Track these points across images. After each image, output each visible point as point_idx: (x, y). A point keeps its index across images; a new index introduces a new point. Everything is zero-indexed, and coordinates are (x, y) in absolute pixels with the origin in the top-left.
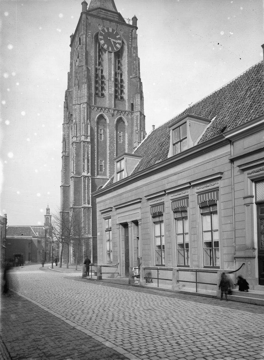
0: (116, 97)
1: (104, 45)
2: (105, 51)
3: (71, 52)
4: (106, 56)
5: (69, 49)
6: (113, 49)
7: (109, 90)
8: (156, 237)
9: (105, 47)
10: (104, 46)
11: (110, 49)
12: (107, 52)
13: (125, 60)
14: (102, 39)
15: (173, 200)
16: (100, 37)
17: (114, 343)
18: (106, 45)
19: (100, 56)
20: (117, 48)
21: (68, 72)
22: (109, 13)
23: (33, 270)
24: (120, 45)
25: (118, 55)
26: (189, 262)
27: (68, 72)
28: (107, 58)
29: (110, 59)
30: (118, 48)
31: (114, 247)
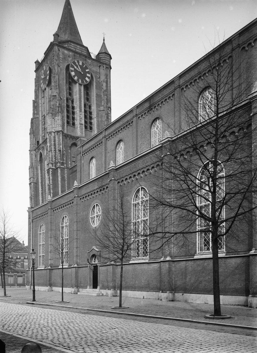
0: (86, 127)
1: (74, 76)
2: (75, 82)
3: (35, 79)
4: (76, 88)
5: (34, 75)
6: (82, 82)
7: (79, 117)
8: (121, 307)
9: (76, 78)
10: (74, 78)
11: (80, 81)
12: (78, 84)
13: (94, 93)
14: (72, 70)
15: (134, 200)
16: (71, 68)
17: (234, 42)
18: (76, 77)
19: (70, 89)
20: (86, 81)
21: (33, 100)
22: (78, 46)
23: (196, 251)
24: (89, 79)
25: (87, 88)
26: (95, 317)
27: (33, 100)
28: (77, 90)
29: (80, 90)
30: (87, 82)
31: (36, 258)
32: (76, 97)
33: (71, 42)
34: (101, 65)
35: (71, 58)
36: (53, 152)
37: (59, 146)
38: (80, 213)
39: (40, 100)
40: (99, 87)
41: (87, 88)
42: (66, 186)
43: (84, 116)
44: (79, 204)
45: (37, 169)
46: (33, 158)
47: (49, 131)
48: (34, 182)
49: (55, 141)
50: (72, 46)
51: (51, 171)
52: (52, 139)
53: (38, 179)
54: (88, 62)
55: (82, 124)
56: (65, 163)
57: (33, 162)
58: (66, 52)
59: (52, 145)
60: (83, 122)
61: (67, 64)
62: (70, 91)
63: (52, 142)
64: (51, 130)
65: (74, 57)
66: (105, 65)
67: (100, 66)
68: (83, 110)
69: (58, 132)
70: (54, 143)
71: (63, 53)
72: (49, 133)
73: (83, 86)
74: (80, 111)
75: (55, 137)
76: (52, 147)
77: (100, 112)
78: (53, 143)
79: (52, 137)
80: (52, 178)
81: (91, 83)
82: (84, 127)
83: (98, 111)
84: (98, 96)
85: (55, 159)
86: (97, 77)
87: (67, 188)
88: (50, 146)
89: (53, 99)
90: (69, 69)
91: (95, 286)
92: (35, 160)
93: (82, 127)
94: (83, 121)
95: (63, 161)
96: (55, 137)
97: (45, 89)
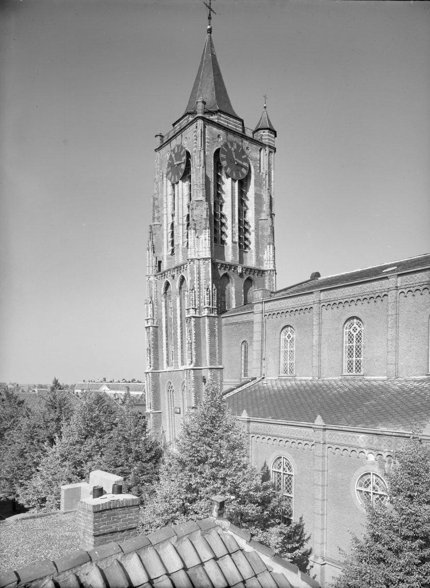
6: (237, 175)
18: (229, 169)
20: (242, 174)
25: (243, 184)
32: (227, 198)
33: (219, 111)
35: (222, 139)
36: (196, 290)
37: (206, 282)
38: (327, 471)
42: (217, 344)
45: (160, 307)
47: (190, 258)
48: (154, 325)
49: (199, 273)
50: (222, 118)
51: (194, 322)
52: (195, 269)
53: (160, 320)
54: (245, 144)
56: (215, 308)
59: (195, 279)
60: (237, 239)
61: (217, 148)
63: (195, 276)
67: (260, 151)
68: (237, 221)
70: (198, 276)
71: (211, 132)
73: (237, 182)
75: (199, 268)
76: (195, 282)
77: (260, 222)
78: (196, 276)
79: (195, 266)
80: (194, 332)
81: (248, 177)
83: (257, 221)
84: (258, 197)
85: (199, 301)
89: (197, 206)
90: (219, 156)
92: (155, 290)
93: (236, 247)
95: (212, 306)
96: (199, 268)
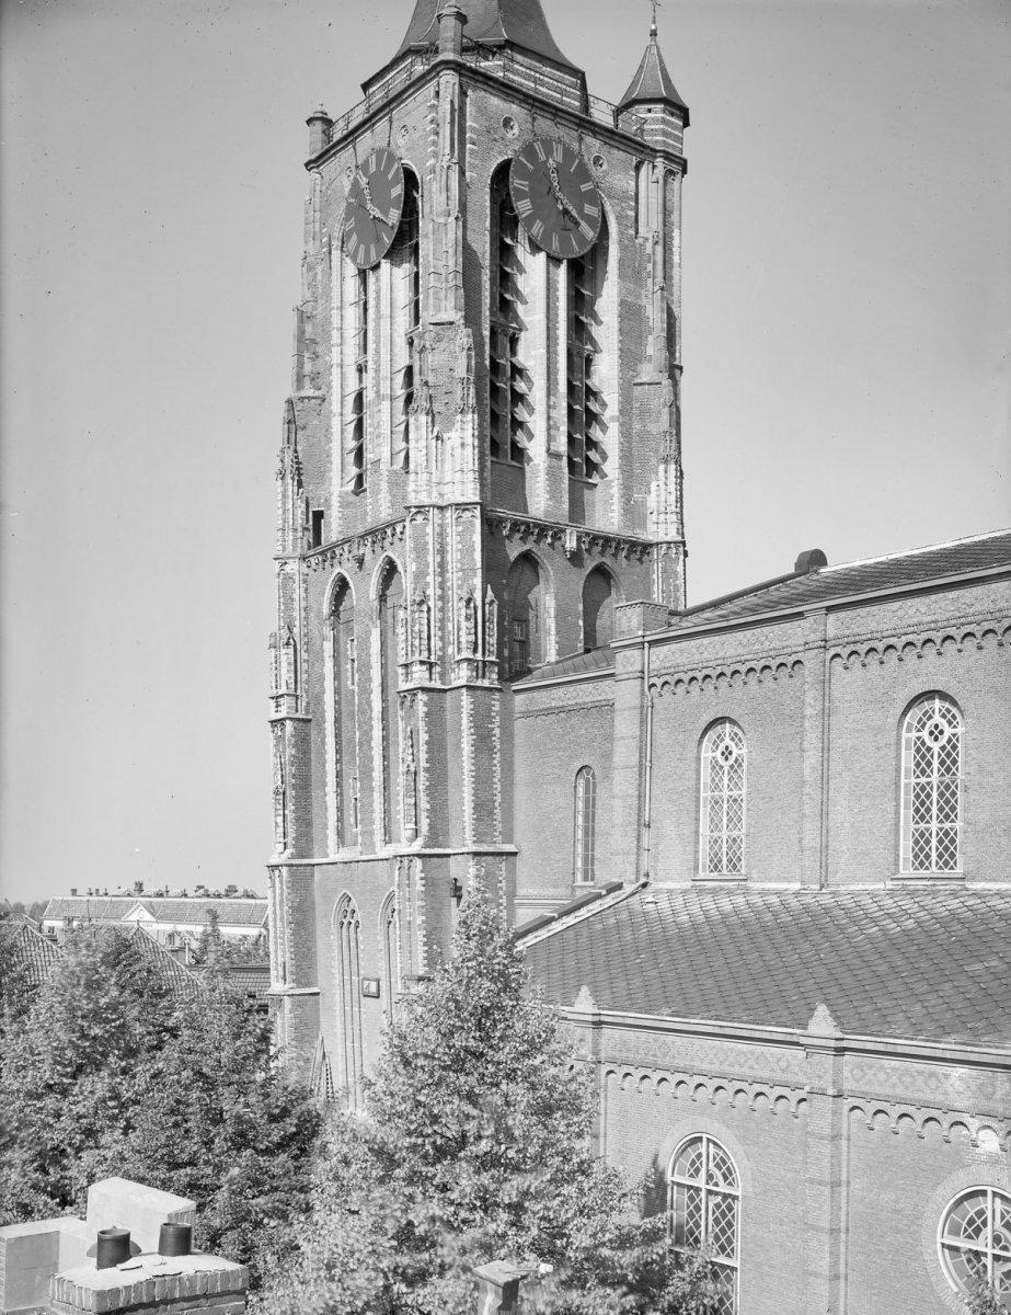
6: (564, 242)
11: (555, 244)
20: (582, 239)
25: (583, 271)
32: (531, 315)
34: (642, 156)
37: (465, 579)
39: (334, 312)
40: (632, 272)
41: (583, 271)
42: (498, 775)
43: (565, 412)
44: (845, 1132)
46: (296, 596)
48: (298, 715)
49: (442, 551)
51: (425, 704)
52: (430, 539)
54: (588, 147)
55: (558, 456)
57: (296, 614)
58: (495, 102)
59: (431, 570)
60: (562, 445)
62: (507, 291)
64: (424, 499)
65: (529, 126)
66: (665, 158)
68: (563, 388)
69: (462, 507)
70: (438, 559)
71: (482, 110)
72: (414, 510)
73: (565, 262)
74: (550, 391)
78: (432, 560)
81: (599, 250)
82: (566, 470)
83: (628, 387)
84: (630, 313)
86: (627, 216)
87: (498, 786)
88: (420, 576)
90: (507, 186)
91: (267, 970)
92: (303, 604)
93: (560, 468)
94: (564, 439)
96: (442, 535)
97: (376, 267)
